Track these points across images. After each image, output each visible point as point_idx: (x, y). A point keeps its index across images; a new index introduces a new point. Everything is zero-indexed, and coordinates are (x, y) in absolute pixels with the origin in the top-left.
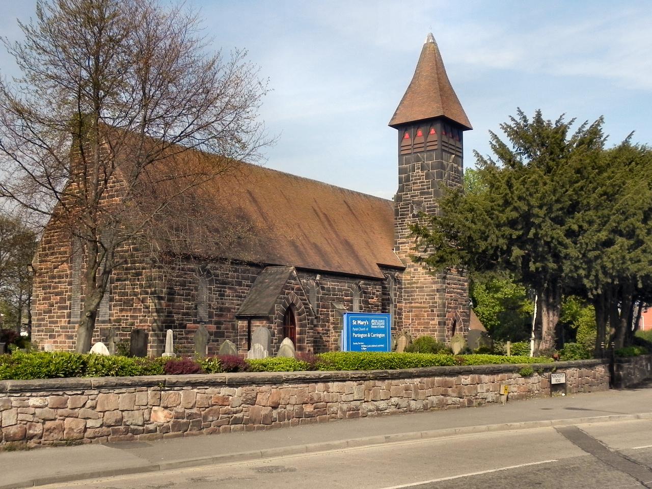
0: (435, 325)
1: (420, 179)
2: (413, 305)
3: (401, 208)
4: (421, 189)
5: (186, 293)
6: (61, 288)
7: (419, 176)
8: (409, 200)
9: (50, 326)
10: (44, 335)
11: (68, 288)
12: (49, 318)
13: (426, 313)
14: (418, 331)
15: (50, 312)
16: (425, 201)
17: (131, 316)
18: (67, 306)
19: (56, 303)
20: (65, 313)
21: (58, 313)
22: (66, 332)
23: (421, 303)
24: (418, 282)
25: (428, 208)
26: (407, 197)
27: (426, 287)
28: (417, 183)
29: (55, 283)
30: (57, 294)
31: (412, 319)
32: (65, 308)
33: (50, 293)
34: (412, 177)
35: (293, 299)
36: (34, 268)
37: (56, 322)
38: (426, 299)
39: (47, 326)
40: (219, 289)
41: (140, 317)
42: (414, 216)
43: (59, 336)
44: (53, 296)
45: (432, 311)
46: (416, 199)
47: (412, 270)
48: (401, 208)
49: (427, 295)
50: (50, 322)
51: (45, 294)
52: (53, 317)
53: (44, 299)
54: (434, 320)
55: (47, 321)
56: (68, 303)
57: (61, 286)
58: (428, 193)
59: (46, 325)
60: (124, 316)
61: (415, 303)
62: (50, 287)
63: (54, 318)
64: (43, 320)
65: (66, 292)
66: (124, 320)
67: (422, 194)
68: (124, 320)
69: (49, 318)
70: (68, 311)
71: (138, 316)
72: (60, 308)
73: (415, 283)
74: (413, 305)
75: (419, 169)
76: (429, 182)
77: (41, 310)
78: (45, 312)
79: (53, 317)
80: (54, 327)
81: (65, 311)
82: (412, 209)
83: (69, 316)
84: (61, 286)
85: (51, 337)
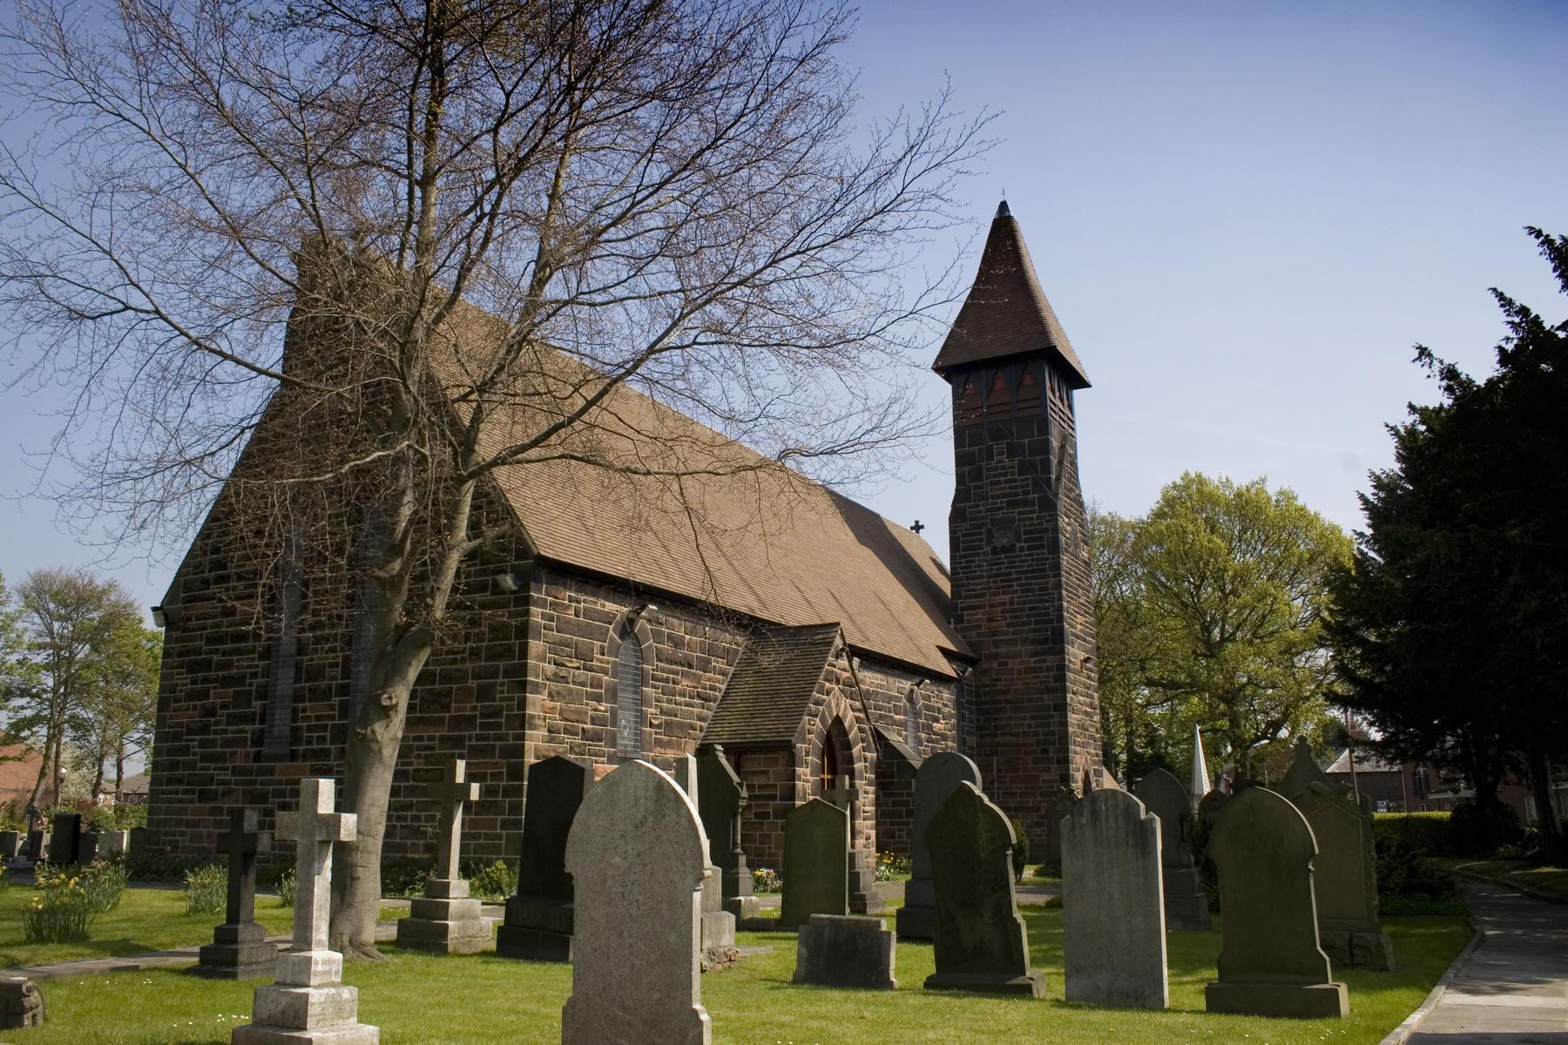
0: (1051, 781)
1: (1006, 474)
2: (999, 739)
3: (964, 536)
4: (1009, 495)
5: (592, 679)
6: (237, 668)
7: (1003, 468)
8: (983, 518)
9: (202, 769)
10: (186, 792)
11: (258, 666)
12: (202, 744)
13: (1030, 757)
14: (1013, 795)
15: (204, 729)
16: (1019, 520)
17: (443, 739)
18: (255, 713)
19: (224, 706)
20: (246, 732)
21: (226, 731)
22: (246, 783)
23: (1017, 735)
24: (1008, 691)
25: (1026, 533)
26: (980, 512)
27: (1029, 701)
28: (999, 483)
29: (224, 653)
30: (227, 682)
31: (999, 771)
32: (247, 719)
33: (206, 680)
34: (988, 470)
35: (838, 705)
36: (244, 933)
37: (221, 757)
38: (1029, 726)
39: (195, 769)
40: (665, 675)
41: (470, 740)
42: (995, 551)
43: (227, 793)
44: (215, 688)
45: (1045, 751)
46: (1000, 514)
47: (995, 665)
48: (964, 536)
49: (1032, 718)
50: (204, 758)
51: (194, 682)
52: (213, 743)
53: (190, 696)
54: (1049, 770)
55: (194, 754)
56: (257, 705)
57: (238, 661)
58: (1025, 503)
59: (192, 765)
60: (420, 738)
61: (1004, 735)
62: (207, 665)
63: (216, 746)
64: (185, 751)
65: (254, 675)
66: (420, 748)
67: (1011, 505)
68: (420, 748)
69: (202, 744)
70: (257, 726)
71: (463, 737)
72: (234, 719)
73: (1001, 692)
74: (999, 739)
75: (1001, 453)
76: (1027, 479)
77: (181, 725)
78: (190, 731)
79: (213, 743)
80: (215, 769)
81: (248, 727)
82: (990, 535)
83: (259, 739)
84: (238, 661)
85: (204, 796)
